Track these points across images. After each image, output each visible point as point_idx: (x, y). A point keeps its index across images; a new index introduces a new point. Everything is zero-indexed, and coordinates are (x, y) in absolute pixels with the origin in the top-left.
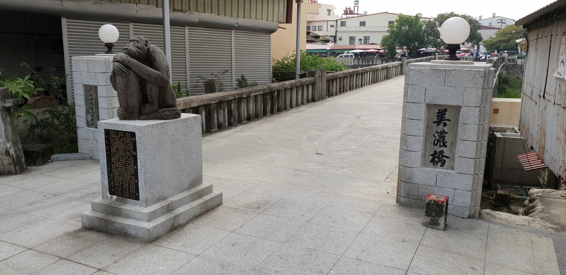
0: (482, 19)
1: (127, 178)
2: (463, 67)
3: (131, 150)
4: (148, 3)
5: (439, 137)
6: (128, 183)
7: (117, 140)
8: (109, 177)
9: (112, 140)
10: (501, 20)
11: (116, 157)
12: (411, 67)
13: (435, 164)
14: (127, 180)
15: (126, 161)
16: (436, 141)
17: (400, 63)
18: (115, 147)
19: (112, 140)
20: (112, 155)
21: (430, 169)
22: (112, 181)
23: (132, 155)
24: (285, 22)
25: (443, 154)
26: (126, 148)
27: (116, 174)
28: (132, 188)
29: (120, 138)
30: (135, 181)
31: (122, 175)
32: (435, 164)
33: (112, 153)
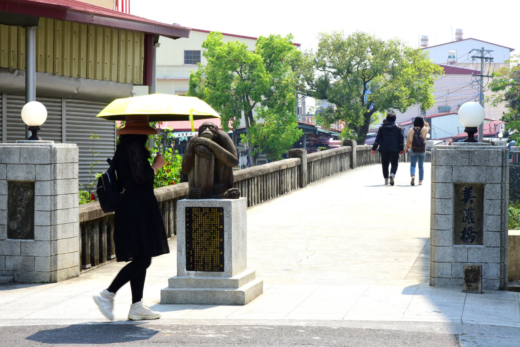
0: (430, 44)
1: (210, 251)
2: (484, 148)
3: (217, 225)
4: (45, 70)
5: (467, 214)
6: (211, 257)
7: (201, 216)
8: (187, 254)
9: (194, 216)
10: (482, 51)
11: (199, 232)
12: (437, 149)
13: (465, 240)
14: (210, 254)
15: (210, 235)
16: (465, 219)
17: (296, 162)
18: (197, 223)
19: (194, 216)
20: (193, 231)
21: (461, 246)
22: (191, 257)
23: (218, 229)
24: (142, 84)
25: (472, 230)
26: (211, 223)
27: (197, 249)
28: (215, 261)
29: (205, 214)
30: (220, 253)
31: (204, 249)
32: (465, 240)
33: (193, 229)
